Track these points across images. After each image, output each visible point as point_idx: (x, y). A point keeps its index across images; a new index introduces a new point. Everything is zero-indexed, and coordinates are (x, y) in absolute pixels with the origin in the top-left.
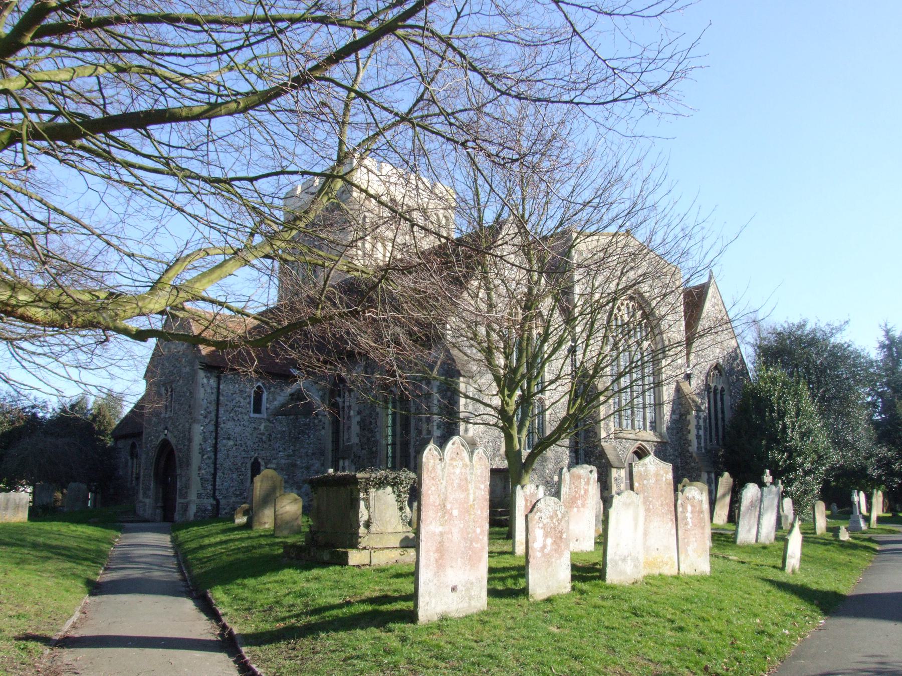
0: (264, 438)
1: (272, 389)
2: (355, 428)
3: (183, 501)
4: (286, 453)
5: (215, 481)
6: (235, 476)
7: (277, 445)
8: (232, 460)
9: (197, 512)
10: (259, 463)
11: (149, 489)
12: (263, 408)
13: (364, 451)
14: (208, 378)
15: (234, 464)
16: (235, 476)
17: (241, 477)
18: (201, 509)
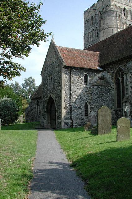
0: (89, 95)
3: (59, 121)
4: (98, 101)
5: (71, 113)
6: (78, 110)
7: (95, 98)
8: (77, 104)
9: (65, 125)
10: (88, 105)
11: (45, 116)
12: (88, 84)
14: (66, 71)
15: (78, 106)
16: (78, 110)
18: (66, 124)
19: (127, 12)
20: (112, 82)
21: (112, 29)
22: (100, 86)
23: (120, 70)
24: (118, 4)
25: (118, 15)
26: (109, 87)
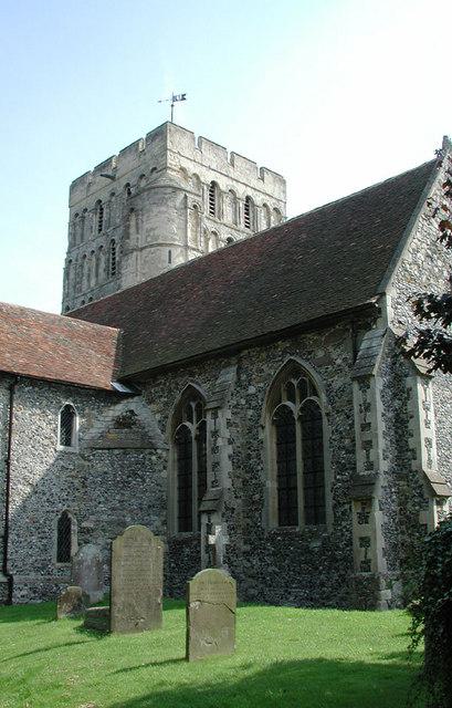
1: (87, 411)
2: (227, 466)
10: (69, 520)
12: (74, 440)
13: (239, 501)
17: (45, 541)
19: (220, 195)
20: (163, 440)
21: (168, 249)
22: (116, 452)
23: (192, 394)
24: (192, 168)
25: (190, 204)
26: (151, 454)
